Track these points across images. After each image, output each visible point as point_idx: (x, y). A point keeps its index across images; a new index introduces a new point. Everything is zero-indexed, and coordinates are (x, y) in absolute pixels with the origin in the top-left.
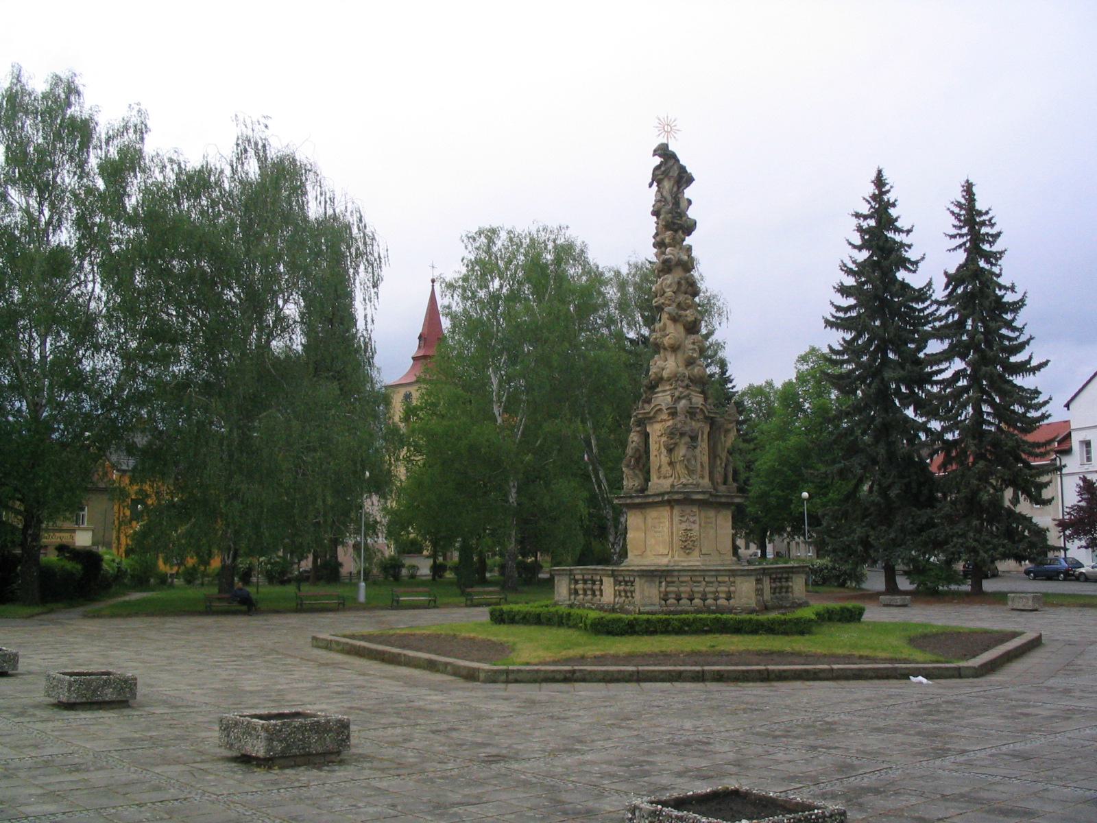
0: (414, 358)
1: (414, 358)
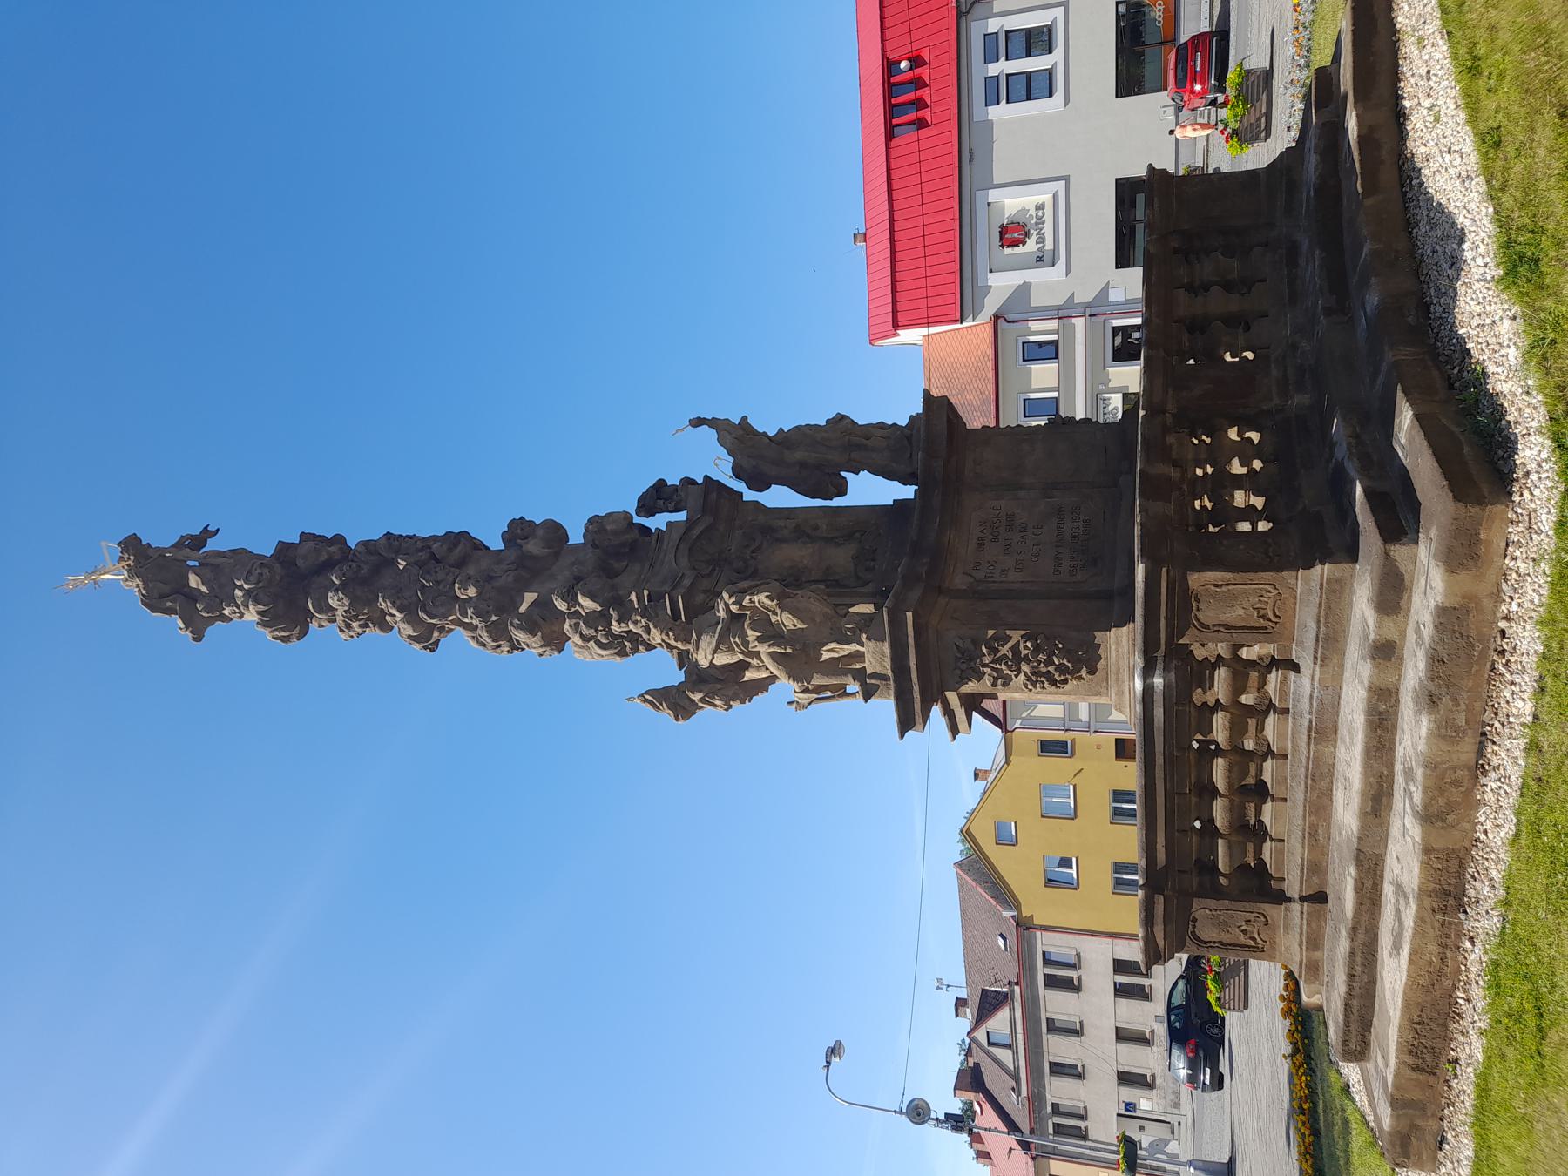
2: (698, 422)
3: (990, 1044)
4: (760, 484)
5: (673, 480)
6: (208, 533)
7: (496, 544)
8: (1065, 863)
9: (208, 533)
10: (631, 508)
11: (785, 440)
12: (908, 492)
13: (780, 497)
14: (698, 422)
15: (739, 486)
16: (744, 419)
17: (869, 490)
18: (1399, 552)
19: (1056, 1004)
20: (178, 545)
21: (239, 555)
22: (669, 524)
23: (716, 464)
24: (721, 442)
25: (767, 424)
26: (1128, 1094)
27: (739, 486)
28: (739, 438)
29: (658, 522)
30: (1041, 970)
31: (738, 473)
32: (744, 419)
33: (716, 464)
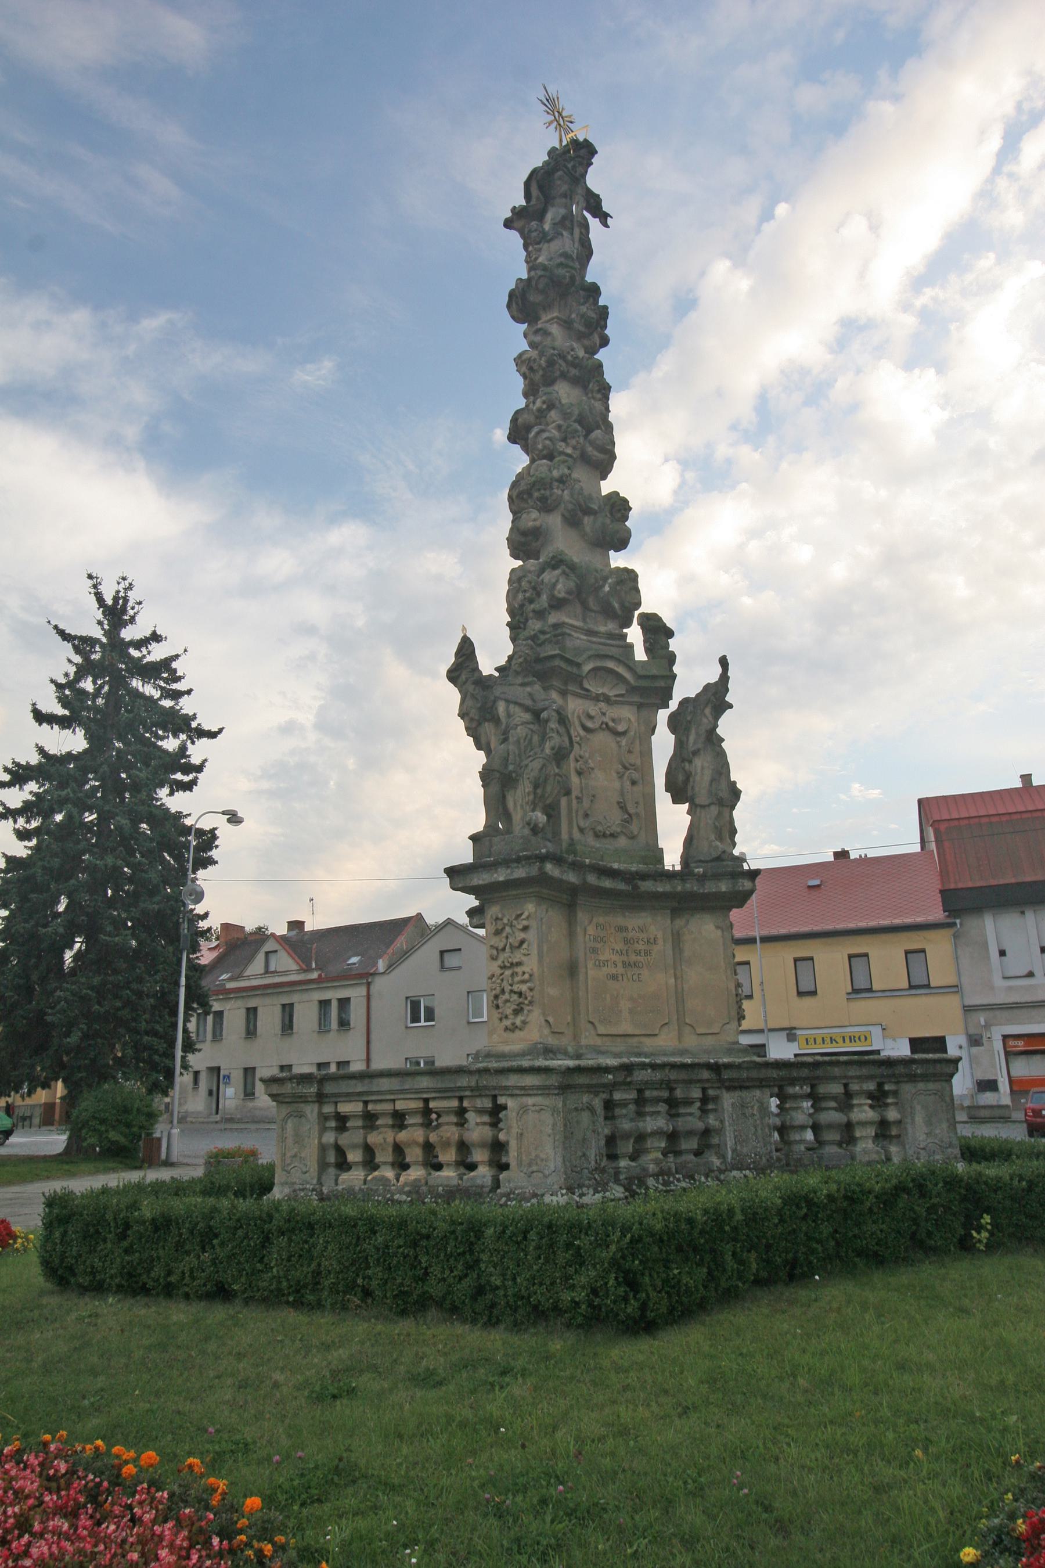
2: (724, 662)
3: (267, 953)
4: (674, 723)
5: (674, 644)
6: (604, 217)
7: (606, 487)
8: (430, 1015)
9: (604, 217)
10: (644, 609)
11: (714, 741)
12: (672, 860)
13: (663, 744)
14: (724, 662)
15: (674, 705)
16: (731, 706)
17: (672, 825)
18: (50, 1101)
19: (306, 1014)
20: (589, 193)
21: (586, 251)
22: (631, 646)
23: (689, 681)
24: (707, 687)
25: (725, 726)
26: (237, 1076)
27: (674, 705)
28: (715, 698)
29: (634, 634)
30: (333, 995)
31: (685, 702)
32: (731, 706)
33: (689, 681)
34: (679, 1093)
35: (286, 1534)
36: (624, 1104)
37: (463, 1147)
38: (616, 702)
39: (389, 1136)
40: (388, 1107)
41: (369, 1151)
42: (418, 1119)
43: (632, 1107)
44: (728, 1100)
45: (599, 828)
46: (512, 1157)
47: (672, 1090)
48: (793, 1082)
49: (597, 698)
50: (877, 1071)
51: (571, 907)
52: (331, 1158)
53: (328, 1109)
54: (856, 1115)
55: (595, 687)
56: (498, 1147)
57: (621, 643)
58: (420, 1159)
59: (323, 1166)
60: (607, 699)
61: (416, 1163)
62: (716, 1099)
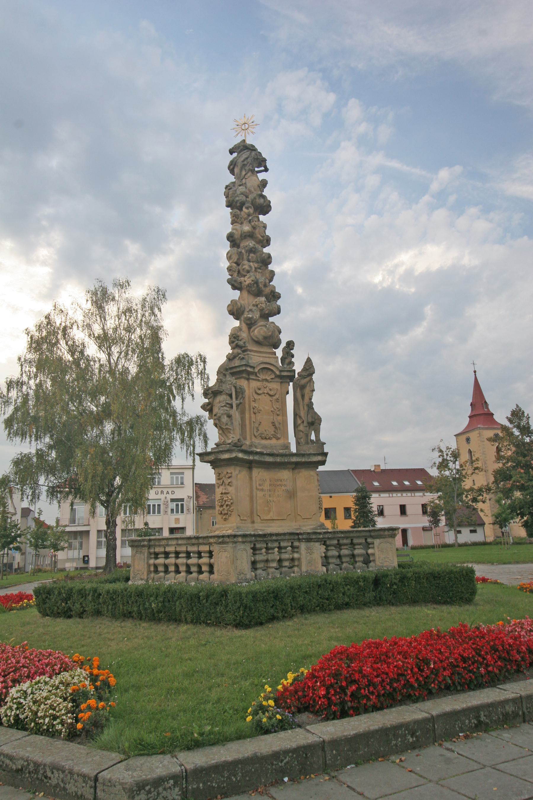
0: (469, 417)
1: (469, 417)
34: (269, 545)
35: (10, 659)
36: (285, 548)
37: (177, 566)
38: (271, 381)
39: (184, 561)
40: (162, 550)
41: (199, 566)
42: (173, 555)
43: (290, 548)
44: (303, 546)
45: (263, 435)
46: (215, 569)
47: (267, 544)
48: (283, 540)
49: (263, 380)
50: (184, 542)
51: (250, 468)
52: (152, 569)
53: (152, 550)
54: (356, 552)
55: (262, 376)
56: (211, 566)
57: (274, 356)
58: (208, 570)
59: (149, 572)
60: (266, 380)
61: (195, 572)
62: (298, 547)
